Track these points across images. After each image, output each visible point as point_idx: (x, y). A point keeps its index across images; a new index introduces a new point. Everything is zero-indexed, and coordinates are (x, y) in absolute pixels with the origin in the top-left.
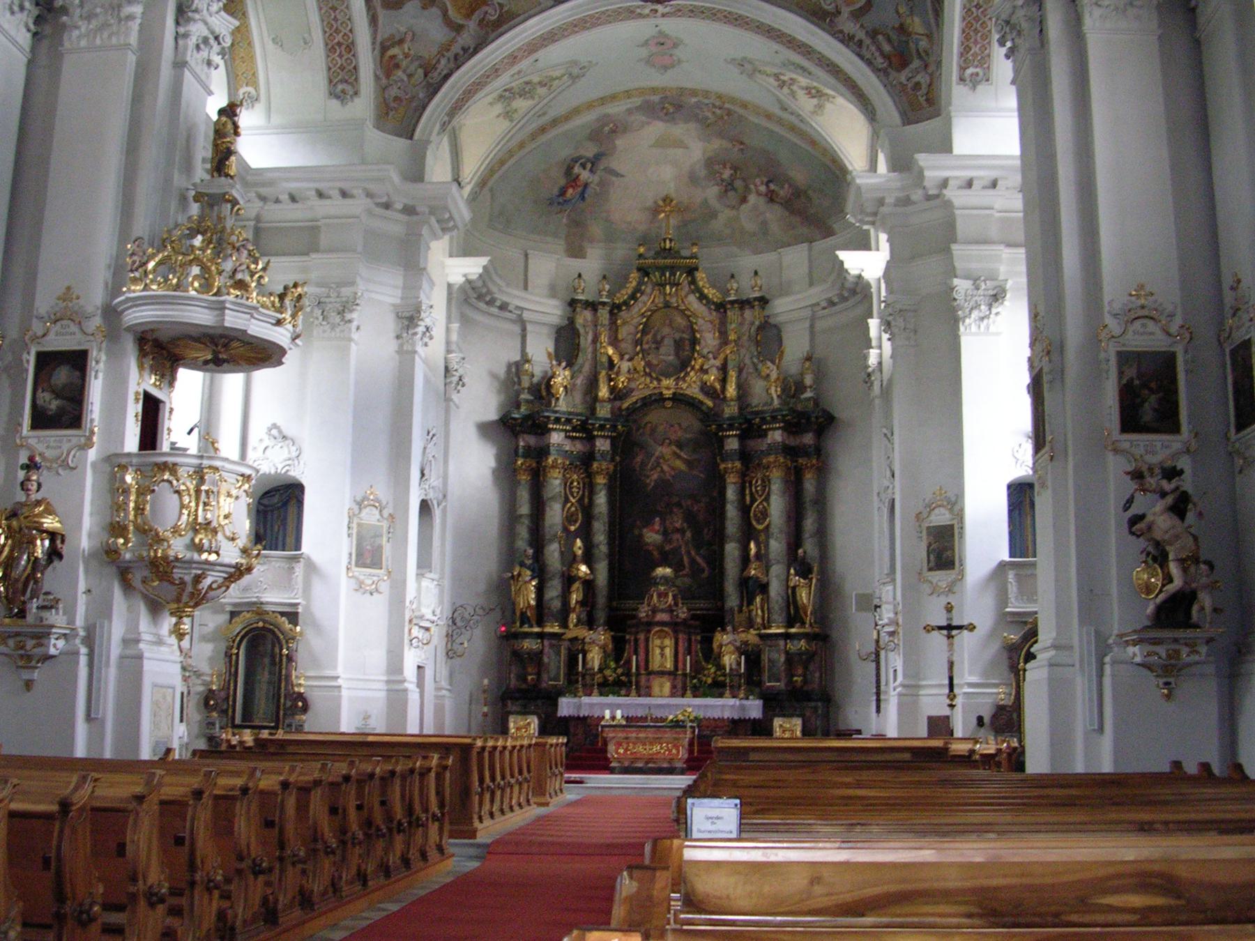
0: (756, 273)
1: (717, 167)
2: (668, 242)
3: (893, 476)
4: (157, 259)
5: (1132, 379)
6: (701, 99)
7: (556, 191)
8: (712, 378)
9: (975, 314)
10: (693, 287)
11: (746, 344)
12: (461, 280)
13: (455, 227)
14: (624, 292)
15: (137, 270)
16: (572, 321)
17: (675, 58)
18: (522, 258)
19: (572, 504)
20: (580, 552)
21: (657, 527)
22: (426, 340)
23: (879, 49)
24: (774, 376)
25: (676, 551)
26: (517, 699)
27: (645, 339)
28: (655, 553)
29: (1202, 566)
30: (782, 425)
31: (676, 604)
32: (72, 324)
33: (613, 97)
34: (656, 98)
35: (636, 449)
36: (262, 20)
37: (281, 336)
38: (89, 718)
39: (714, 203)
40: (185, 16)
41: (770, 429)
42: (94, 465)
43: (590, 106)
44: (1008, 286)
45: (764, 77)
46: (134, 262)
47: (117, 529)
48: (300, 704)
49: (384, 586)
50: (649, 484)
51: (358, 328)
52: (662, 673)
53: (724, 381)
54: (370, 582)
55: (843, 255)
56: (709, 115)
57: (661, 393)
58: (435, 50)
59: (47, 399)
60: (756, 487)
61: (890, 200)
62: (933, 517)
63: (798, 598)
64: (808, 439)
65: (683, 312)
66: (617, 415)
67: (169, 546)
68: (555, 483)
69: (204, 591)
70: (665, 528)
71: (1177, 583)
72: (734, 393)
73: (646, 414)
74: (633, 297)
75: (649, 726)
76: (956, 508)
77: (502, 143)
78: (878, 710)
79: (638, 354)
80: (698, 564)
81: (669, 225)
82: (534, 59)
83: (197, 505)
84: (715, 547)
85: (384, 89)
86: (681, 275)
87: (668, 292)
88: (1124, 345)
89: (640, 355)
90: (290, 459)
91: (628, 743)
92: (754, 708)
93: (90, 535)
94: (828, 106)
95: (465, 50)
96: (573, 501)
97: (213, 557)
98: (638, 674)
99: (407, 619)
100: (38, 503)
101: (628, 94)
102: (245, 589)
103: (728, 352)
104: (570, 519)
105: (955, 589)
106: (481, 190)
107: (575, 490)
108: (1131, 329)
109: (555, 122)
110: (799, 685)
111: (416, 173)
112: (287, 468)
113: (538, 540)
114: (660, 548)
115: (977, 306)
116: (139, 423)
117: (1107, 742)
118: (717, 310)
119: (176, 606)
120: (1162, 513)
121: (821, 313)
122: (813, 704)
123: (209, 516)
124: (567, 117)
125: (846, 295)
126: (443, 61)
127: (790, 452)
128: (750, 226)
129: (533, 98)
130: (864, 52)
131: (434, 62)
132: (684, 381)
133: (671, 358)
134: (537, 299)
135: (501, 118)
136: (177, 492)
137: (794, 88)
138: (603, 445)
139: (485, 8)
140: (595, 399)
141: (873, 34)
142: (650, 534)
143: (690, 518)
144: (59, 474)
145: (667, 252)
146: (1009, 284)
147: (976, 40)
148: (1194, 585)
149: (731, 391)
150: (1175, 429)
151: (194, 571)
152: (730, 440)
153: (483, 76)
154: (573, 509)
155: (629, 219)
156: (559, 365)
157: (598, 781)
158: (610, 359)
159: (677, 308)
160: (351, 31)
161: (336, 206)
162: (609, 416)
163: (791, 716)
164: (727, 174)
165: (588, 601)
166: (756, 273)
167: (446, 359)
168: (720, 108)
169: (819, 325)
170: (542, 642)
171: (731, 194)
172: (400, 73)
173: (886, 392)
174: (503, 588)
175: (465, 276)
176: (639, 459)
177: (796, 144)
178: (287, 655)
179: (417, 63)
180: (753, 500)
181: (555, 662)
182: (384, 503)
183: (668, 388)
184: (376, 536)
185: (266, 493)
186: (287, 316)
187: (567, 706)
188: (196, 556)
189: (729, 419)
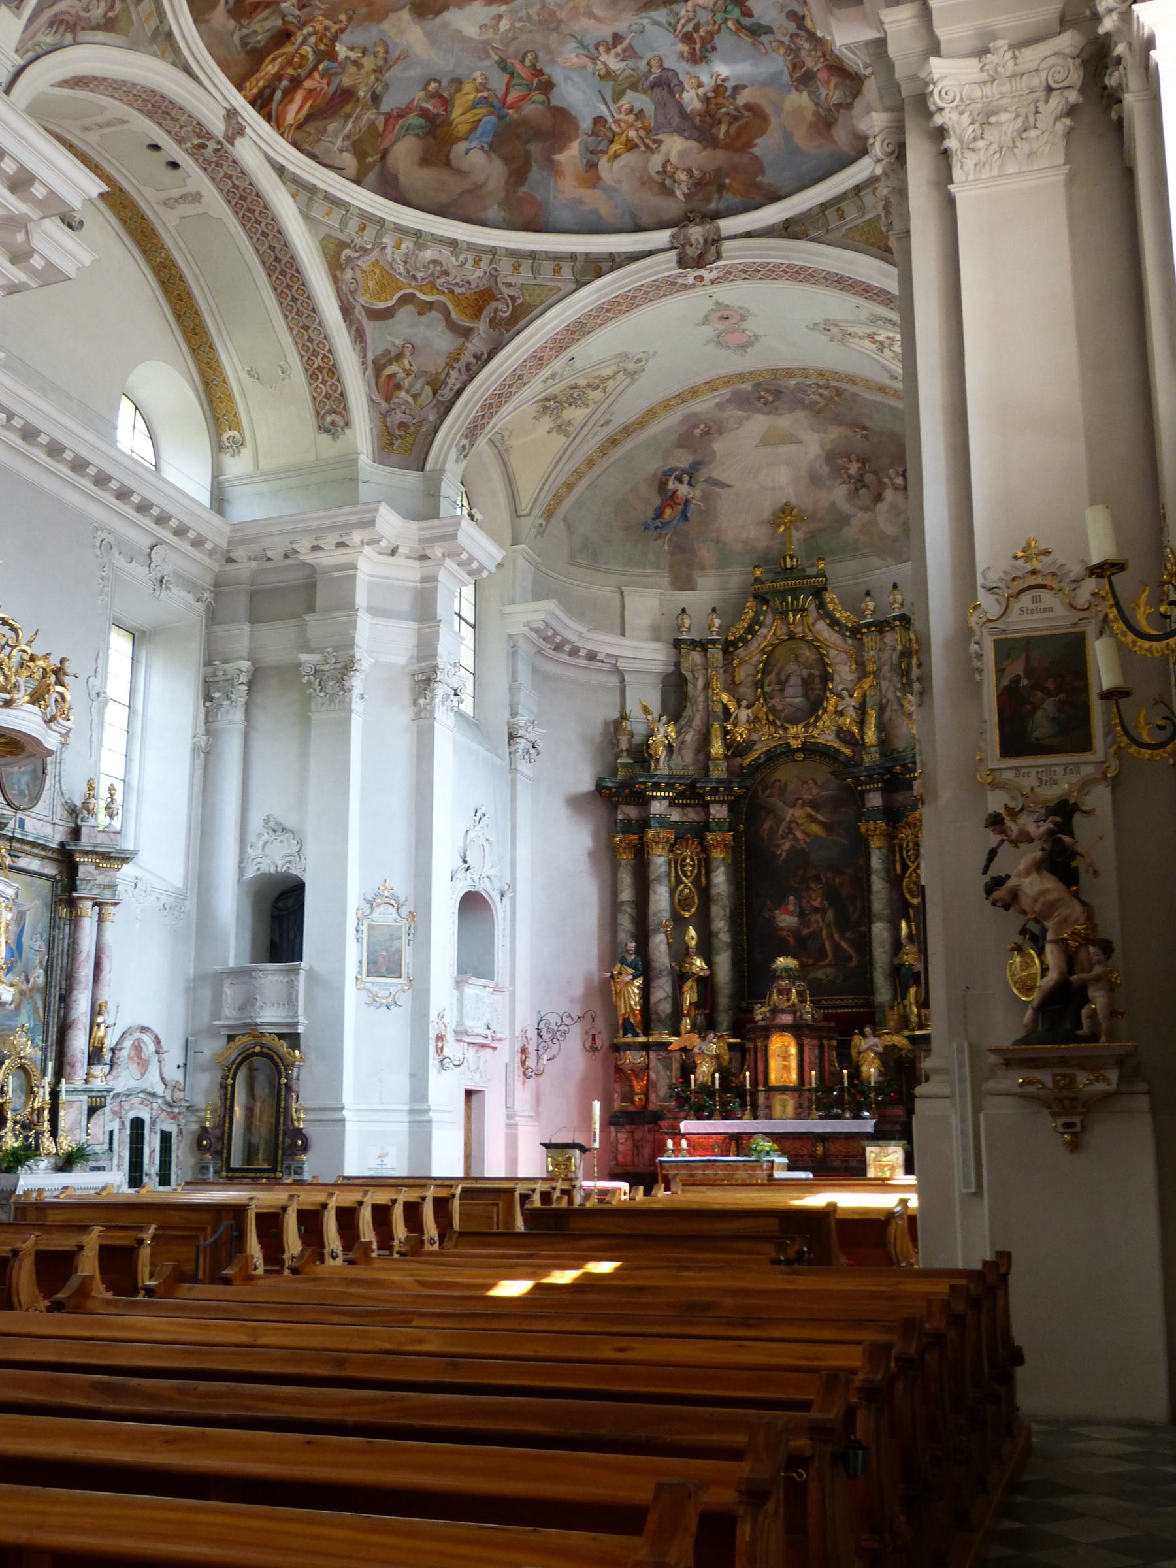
1: (840, 461)
2: (788, 559)
5: (1018, 677)
7: (651, 514)
11: (888, 675)
14: (739, 625)
18: (617, 597)
21: (791, 907)
25: (816, 935)
26: (622, 1125)
27: (768, 680)
28: (790, 939)
33: (694, 392)
34: (747, 386)
36: (232, 352)
39: (844, 506)
43: (667, 405)
45: (857, 340)
48: (300, 1142)
49: (405, 999)
53: (861, 723)
54: (387, 993)
56: (817, 398)
57: (788, 744)
58: (442, 361)
60: (908, 851)
65: (810, 643)
68: (660, 861)
74: (750, 630)
79: (758, 699)
80: (845, 951)
82: (569, 356)
84: (863, 929)
86: (805, 599)
88: (1004, 631)
89: (762, 701)
95: (477, 357)
99: (432, 1035)
101: (711, 385)
103: (866, 687)
104: (685, 903)
108: (1016, 606)
109: (628, 430)
113: (642, 934)
114: (796, 933)
118: (853, 637)
124: (641, 423)
126: (454, 374)
129: (587, 405)
131: (443, 376)
132: (816, 727)
138: (719, 812)
139: (494, 304)
140: (708, 757)
143: (831, 894)
149: (871, 735)
150: (1085, 745)
152: (871, 795)
153: (502, 385)
158: (725, 706)
159: (803, 639)
160: (330, 351)
164: (854, 468)
168: (827, 388)
170: (648, 1055)
171: (862, 492)
172: (403, 394)
175: (527, 624)
176: (766, 826)
178: (286, 1084)
179: (421, 381)
182: (402, 899)
184: (392, 939)
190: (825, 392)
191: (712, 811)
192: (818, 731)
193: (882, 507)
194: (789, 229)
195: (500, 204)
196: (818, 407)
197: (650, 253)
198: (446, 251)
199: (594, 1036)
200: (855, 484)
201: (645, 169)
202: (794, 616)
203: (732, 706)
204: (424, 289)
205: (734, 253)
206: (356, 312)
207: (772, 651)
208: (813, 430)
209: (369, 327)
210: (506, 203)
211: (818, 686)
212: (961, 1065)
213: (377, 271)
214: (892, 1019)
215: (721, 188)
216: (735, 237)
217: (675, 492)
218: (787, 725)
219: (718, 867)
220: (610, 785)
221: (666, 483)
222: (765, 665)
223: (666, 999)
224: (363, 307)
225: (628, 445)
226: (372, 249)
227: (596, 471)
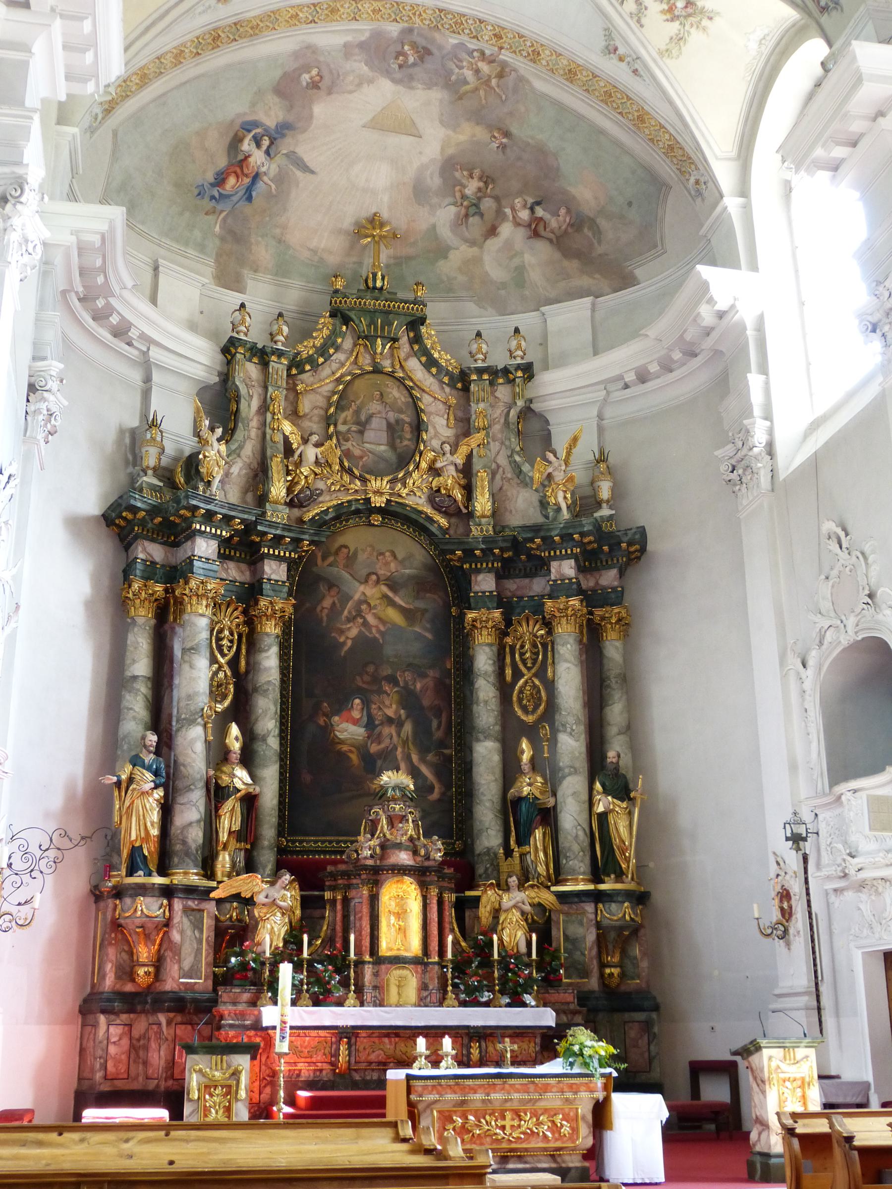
7: (210, 177)
8: (450, 479)
10: (416, 347)
20: (236, 746)
21: (356, 714)
26: (117, 1014)
28: (354, 757)
35: (323, 588)
39: (446, 233)
41: (555, 558)
50: (344, 643)
53: (468, 490)
57: (368, 501)
60: (522, 655)
63: (612, 827)
64: (609, 578)
65: (400, 381)
72: (489, 506)
73: (341, 533)
74: (323, 351)
79: (330, 438)
80: (426, 778)
87: (379, 350)
89: (334, 440)
92: (547, 1018)
98: (359, 963)
103: (474, 445)
104: (216, 691)
107: (225, 642)
110: (615, 980)
118: (452, 385)
121: (618, 395)
132: (404, 485)
133: (383, 448)
142: (344, 725)
143: (408, 700)
152: (480, 577)
154: (221, 675)
155: (313, 244)
156: (212, 429)
158: (286, 439)
159: (391, 375)
164: (472, 187)
170: (170, 905)
171: (474, 220)
175: (75, 232)
176: (327, 603)
177: (601, 132)
180: (517, 674)
183: (378, 492)
190: (484, 67)
191: (267, 569)
192: (406, 491)
193: (493, 244)
200: (467, 208)
203: (295, 441)
207: (350, 382)
208: (441, 122)
211: (408, 436)
217: (247, 158)
218: (368, 476)
219: (270, 647)
220: (139, 505)
221: (241, 140)
222: (340, 398)
223: (198, 821)
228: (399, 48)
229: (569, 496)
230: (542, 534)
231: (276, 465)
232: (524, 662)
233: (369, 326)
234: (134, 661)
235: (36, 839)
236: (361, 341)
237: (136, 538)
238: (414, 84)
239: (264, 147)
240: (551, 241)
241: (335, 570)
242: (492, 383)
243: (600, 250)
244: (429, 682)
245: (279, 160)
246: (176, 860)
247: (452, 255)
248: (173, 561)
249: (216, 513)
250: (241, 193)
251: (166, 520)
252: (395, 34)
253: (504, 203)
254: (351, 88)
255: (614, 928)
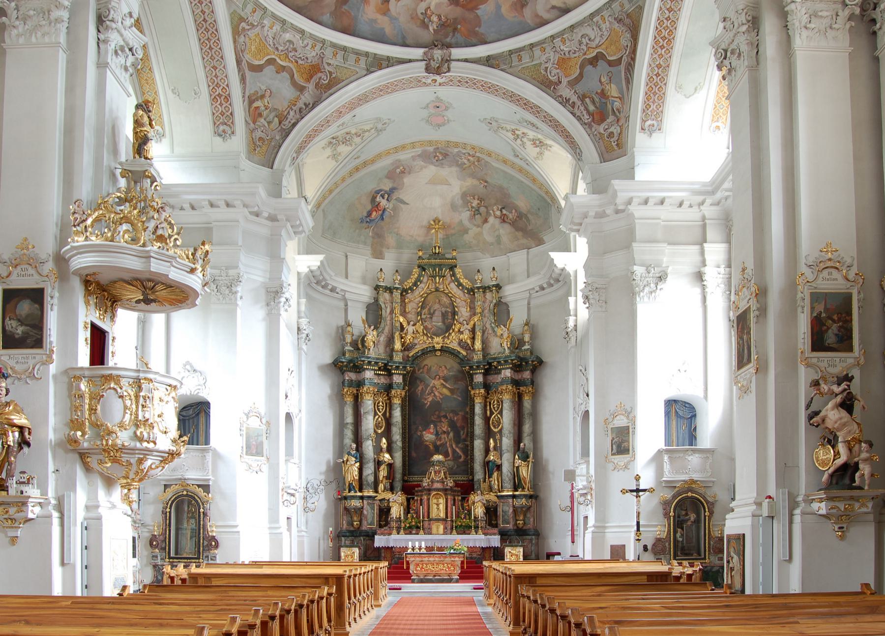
0: (494, 269)
3: (588, 395)
4: (94, 217)
5: (821, 312)
6: (461, 149)
7: (365, 214)
8: (466, 336)
9: (647, 289)
12: (306, 270)
13: (303, 231)
14: (409, 281)
15: (78, 225)
16: (376, 300)
17: (446, 119)
18: (344, 257)
19: (379, 416)
20: (385, 446)
21: (432, 430)
22: (286, 307)
23: (586, 109)
24: (506, 335)
26: (348, 537)
27: (423, 312)
28: (431, 446)
29: (863, 445)
30: (511, 366)
31: (446, 478)
32: (30, 268)
33: (403, 147)
35: (418, 382)
37: (195, 281)
38: (63, 563)
39: (466, 223)
40: (104, 25)
41: (503, 369)
42: (55, 377)
43: (388, 153)
44: (669, 271)
45: (504, 132)
46: (76, 219)
47: (75, 424)
48: (213, 543)
49: (265, 468)
51: (241, 298)
52: (438, 520)
53: (473, 338)
55: (553, 255)
56: (466, 161)
59: (14, 326)
60: (493, 405)
61: (592, 214)
62: (615, 422)
63: (521, 473)
64: (527, 375)
66: (406, 359)
67: (117, 437)
68: (368, 403)
69: (145, 470)
70: (437, 431)
71: (843, 459)
72: (480, 346)
74: (415, 284)
75: (436, 554)
76: (631, 416)
77: (331, 177)
78: (573, 542)
81: (437, 238)
82: (353, 115)
83: (137, 407)
85: (252, 131)
87: (438, 281)
89: (420, 322)
90: (199, 385)
91: (423, 564)
92: (495, 541)
93: (55, 430)
94: (546, 153)
96: (380, 414)
97: (151, 446)
100: (8, 404)
101: (413, 145)
102: (174, 470)
103: (476, 320)
104: (377, 426)
105: (629, 467)
106: (317, 210)
109: (365, 164)
110: (521, 526)
111: (276, 191)
112: (198, 391)
113: (358, 440)
115: (648, 284)
116: (89, 346)
117: (795, 570)
118: (469, 293)
119: (125, 481)
120: (833, 409)
122: (529, 537)
123: (147, 416)
124: (373, 161)
125: (552, 282)
126: (292, 113)
127: (516, 383)
128: (489, 238)
130: (576, 110)
131: (286, 113)
132: (449, 339)
134: (354, 285)
135: (330, 159)
136: (121, 397)
137: (525, 140)
138: (398, 379)
139: (319, 75)
140: (393, 350)
141: (582, 98)
143: (452, 424)
144: (27, 383)
145: (435, 255)
146: (669, 270)
147: (654, 100)
148: (856, 460)
149: (478, 345)
150: (850, 349)
151: (137, 456)
152: (477, 376)
154: (380, 419)
157: (408, 587)
158: (401, 324)
159: (443, 292)
160: (227, 85)
161: (222, 213)
162: (402, 361)
163: (516, 546)
164: (475, 203)
165: (390, 476)
166: (494, 269)
167: (298, 322)
169: (532, 303)
170: (363, 502)
172: (262, 120)
173: (581, 344)
174: (337, 470)
175: (309, 267)
176: (420, 388)
177: (522, 182)
179: (273, 114)
180: (492, 413)
181: (371, 514)
183: (438, 343)
184: (258, 436)
185: (184, 408)
186: (199, 267)
187: (380, 541)
188: (138, 445)
189: (477, 362)
191: (394, 378)
192: (449, 341)
193: (487, 226)
194: (489, 61)
195: (331, 13)
196: (465, 166)
197: (410, 61)
198: (298, 36)
199: (339, 491)
200: (474, 212)
201: (415, 10)
202: (440, 279)
203: (405, 324)
204: (281, 57)
205: (458, 70)
206: (243, 64)
209: (248, 74)
210: (334, 14)
211: (450, 318)
212: (784, 501)
213: (258, 41)
214: (484, 486)
215: (455, 30)
216: (458, 60)
218: (434, 336)
220: (344, 360)
221: (376, 198)
223: (372, 474)
224: (247, 61)
225: (363, 172)
226: (257, 26)
227: (345, 184)
228: (435, 154)
229: (509, 343)
230: (497, 360)
231: (397, 335)
232: (494, 408)
233: (433, 272)
234: (347, 418)
235: (316, 483)
236: (430, 279)
237: (345, 371)
238: (444, 166)
239: (386, 198)
240: (510, 224)
241: (423, 375)
242: (484, 292)
243: (530, 228)
244: (460, 417)
245: (393, 202)
246: (364, 487)
247: (470, 232)
248: (359, 379)
249: (371, 362)
250: (379, 218)
251: (354, 364)
252: (432, 150)
253: (489, 209)
254: (418, 170)
255: (519, 507)
